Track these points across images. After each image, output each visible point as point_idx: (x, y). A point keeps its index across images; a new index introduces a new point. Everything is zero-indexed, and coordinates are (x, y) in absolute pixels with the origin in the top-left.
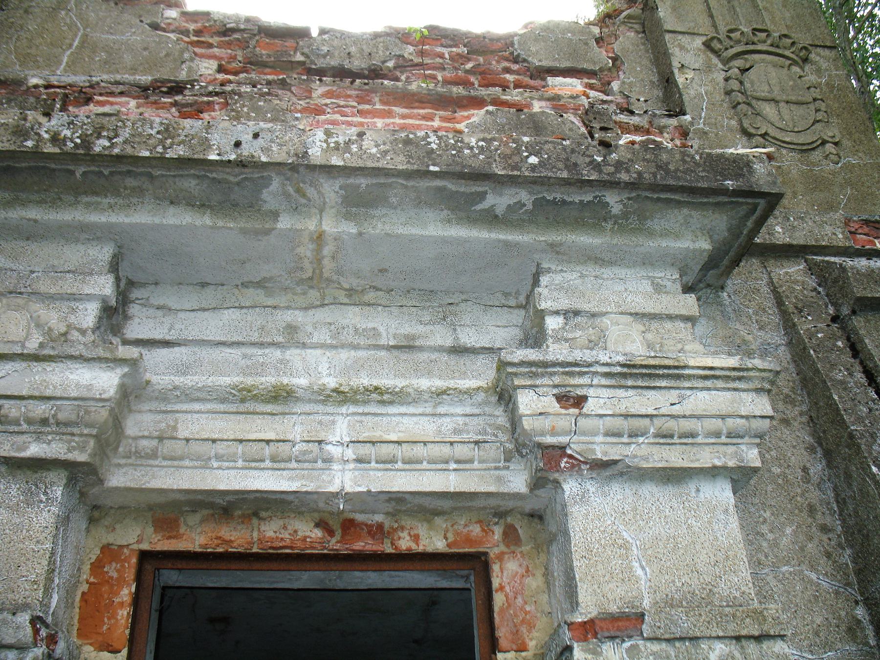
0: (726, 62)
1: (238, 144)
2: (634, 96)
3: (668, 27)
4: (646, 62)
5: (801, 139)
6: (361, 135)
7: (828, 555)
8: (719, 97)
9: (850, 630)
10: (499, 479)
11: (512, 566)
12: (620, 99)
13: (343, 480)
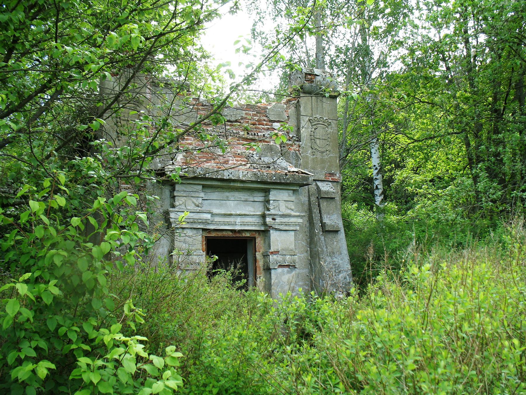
0: (312, 126)
4: (295, 118)
8: (308, 136)
11: (259, 239)
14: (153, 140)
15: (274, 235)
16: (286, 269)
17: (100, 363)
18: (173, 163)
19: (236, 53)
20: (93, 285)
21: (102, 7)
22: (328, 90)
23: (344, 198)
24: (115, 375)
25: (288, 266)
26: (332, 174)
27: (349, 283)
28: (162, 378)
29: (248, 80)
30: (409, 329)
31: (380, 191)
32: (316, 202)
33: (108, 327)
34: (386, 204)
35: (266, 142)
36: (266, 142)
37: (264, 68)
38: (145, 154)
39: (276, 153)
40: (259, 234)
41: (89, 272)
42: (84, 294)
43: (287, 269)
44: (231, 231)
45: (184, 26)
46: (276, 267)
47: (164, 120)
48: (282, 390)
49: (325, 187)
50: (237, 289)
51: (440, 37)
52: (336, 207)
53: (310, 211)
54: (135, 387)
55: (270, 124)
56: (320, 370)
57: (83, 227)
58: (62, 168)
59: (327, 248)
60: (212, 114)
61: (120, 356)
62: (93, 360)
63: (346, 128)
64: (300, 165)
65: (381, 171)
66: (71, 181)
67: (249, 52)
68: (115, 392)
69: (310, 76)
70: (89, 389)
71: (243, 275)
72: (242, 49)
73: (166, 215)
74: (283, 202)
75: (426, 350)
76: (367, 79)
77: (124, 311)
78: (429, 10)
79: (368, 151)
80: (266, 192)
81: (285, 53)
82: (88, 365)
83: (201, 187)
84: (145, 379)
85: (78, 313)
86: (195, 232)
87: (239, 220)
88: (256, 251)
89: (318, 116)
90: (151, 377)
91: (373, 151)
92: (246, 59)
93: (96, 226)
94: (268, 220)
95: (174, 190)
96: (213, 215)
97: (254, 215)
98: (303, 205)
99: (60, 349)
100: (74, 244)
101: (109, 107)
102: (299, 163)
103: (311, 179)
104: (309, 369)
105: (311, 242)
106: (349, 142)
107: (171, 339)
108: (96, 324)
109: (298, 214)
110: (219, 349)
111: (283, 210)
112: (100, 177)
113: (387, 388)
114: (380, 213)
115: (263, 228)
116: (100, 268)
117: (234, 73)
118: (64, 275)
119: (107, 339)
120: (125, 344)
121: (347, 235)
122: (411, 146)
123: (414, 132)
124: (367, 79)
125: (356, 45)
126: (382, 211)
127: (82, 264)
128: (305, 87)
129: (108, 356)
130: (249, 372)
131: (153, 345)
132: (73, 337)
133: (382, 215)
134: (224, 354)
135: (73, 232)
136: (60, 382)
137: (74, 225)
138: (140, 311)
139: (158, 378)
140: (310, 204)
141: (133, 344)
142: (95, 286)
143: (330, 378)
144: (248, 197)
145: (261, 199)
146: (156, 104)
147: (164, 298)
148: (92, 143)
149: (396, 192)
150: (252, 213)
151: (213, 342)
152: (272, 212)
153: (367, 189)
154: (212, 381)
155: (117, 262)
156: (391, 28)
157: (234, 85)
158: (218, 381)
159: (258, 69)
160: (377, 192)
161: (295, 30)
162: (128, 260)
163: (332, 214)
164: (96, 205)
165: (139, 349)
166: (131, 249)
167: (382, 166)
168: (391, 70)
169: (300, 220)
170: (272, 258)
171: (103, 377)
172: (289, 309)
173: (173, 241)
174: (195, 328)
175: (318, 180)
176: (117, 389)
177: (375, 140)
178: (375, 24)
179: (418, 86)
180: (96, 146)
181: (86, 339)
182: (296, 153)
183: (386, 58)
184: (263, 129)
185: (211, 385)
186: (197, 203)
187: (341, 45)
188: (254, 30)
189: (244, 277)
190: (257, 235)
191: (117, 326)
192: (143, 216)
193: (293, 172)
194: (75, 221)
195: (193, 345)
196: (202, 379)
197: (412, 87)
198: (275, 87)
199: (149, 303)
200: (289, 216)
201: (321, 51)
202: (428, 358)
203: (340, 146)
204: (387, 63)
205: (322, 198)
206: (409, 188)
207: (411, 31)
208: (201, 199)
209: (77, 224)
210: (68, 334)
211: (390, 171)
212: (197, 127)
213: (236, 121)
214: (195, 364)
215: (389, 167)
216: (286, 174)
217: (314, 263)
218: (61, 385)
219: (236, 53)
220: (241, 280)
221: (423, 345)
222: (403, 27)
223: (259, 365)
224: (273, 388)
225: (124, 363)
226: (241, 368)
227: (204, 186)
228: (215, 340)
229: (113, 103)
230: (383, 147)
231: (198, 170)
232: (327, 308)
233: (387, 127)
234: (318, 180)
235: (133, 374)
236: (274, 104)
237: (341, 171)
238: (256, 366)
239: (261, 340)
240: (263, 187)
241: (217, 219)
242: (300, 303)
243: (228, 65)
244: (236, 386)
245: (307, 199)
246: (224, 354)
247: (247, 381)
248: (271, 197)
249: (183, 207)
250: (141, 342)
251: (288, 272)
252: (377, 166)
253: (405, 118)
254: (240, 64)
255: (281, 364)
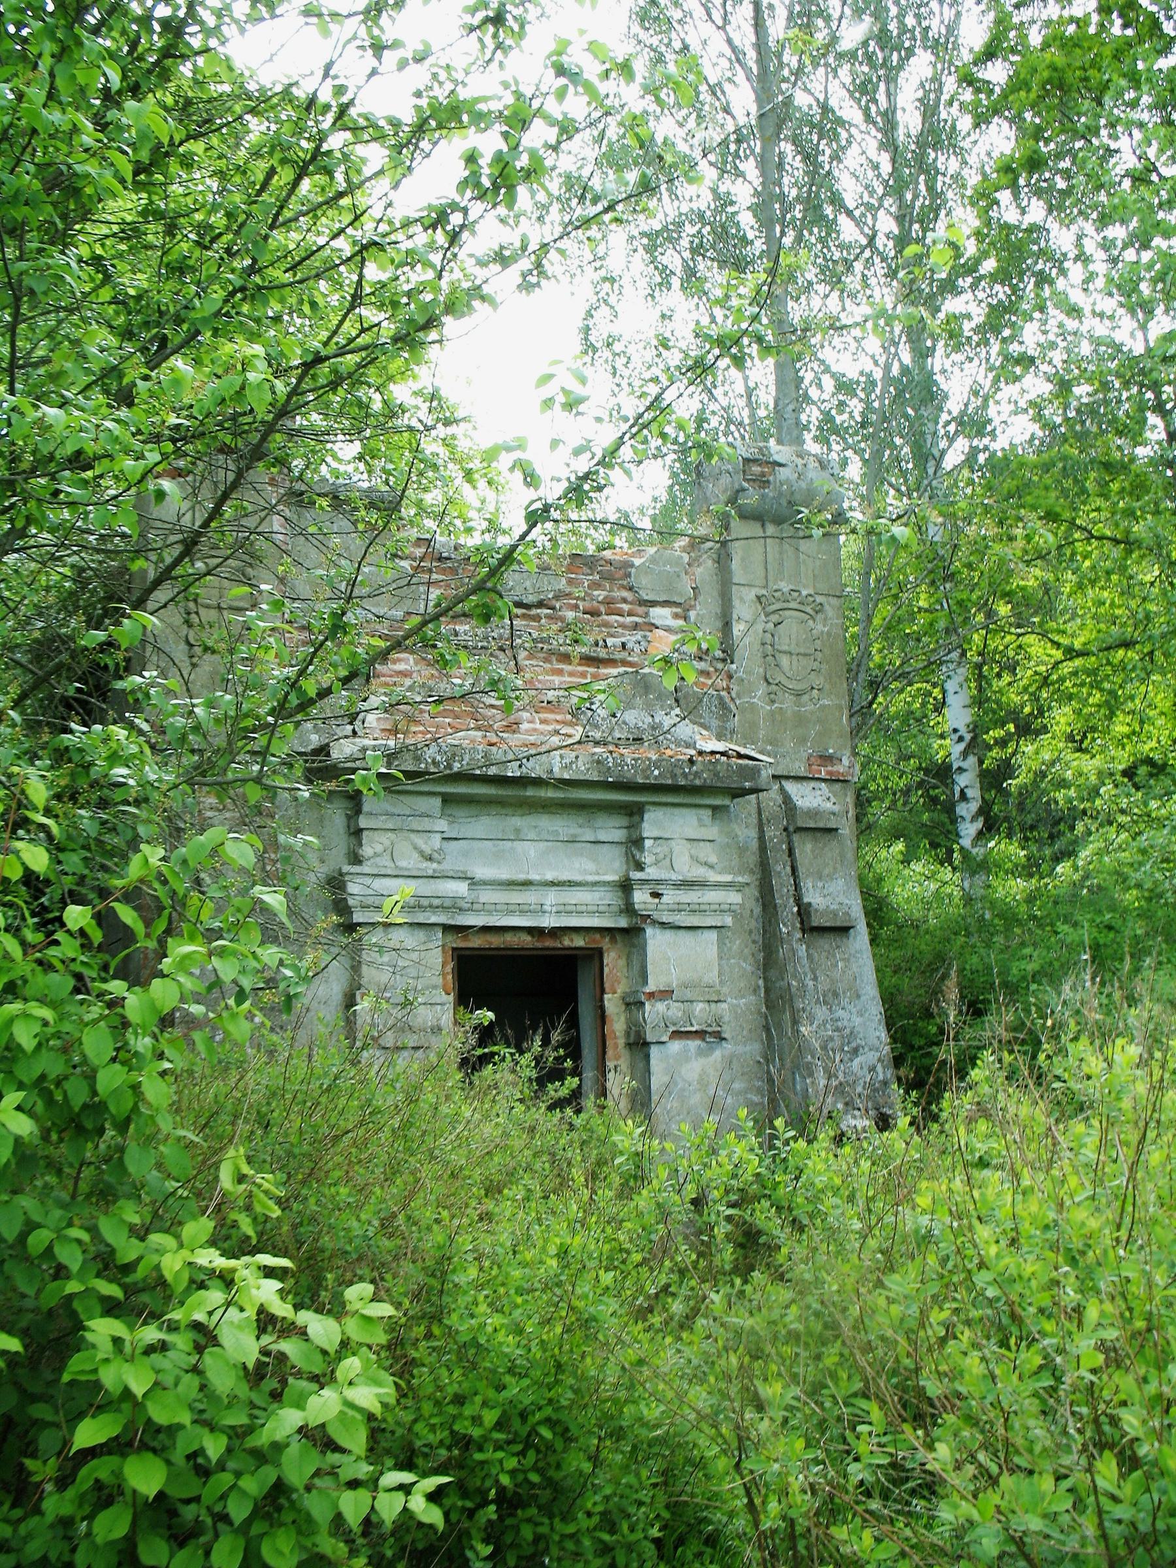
5: (799, 687)
8: (757, 646)
11: (613, 954)
14: (302, 673)
15: (655, 939)
16: (693, 1044)
17: (151, 1334)
18: (354, 733)
19: (543, 412)
20: (130, 1105)
21: (142, 280)
22: (819, 518)
23: (865, 829)
24: (195, 1370)
25: (700, 1034)
26: (827, 759)
27: (885, 1083)
28: (333, 1379)
29: (579, 491)
30: (1077, 1244)
31: (974, 806)
32: (781, 842)
33: (173, 1227)
34: (992, 844)
35: (631, 664)
36: (631, 664)
37: (626, 452)
38: (272, 712)
39: (660, 697)
40: (613, 940)
41: (117, 1066)
42: (101, 1131)
43: (698, 1042)
44: (530, 930)
45: (388, 329)
46: (665, 1038)
47: (333, 614)
48: (687, 1411)
49: (807, 797)
50: (551, 1108)
51: (1146, 341)
52: (842, 856)
53: (764, 870)
54: (253, 1406)
55: (641, 610)
56: (804, 1354)
57: (97, 936)
58: (32, 757)
59: (815, 979)
60: (473, 592)
61: (210, 1313)
62: (131, 1327)
63: (869, 618)
64: (733, 732)
65: (975, 745)
66: (58, 797)
67: (581, 408)
68: (195, 1422)
69: (758, 468)
70: (118, 1410)
71: (568, 1064)
72: (561, 399)
73: (336, 883)
74: (682, 843)
75: (1130, 1309)
76: (931, 471)
77: (217, 1179)
78: (1114, 261)
79: (934, 685)
80: (631, 815)
81: (686, 404)
82: (117, 1341)
83: (437, 802)
84: (284, 1382)
85: (83, 1187)
86: (421, 935)
87: (551, 898)
88: (603, 991)
89: (785, 586)
90: (299, 1374)
91: (950, 686)
92: (574, 429)
93: (139, 927)
94: (640, 897)
95: (358, 811)
96: (473, 883)
97: (595, 884)
98: (742, 850)
99: (31, 1292)
100: (71, 983)
101: (165, 576)
102: (729, 725)
103: (766, 774)
104: (768, 1349)
105: (769, 959)
106: (877, 659)
107: (360, 1259)
108: (136, 1220)
109: (728, 878)
110: (502, 1290)
111: (685, 868)
112: (145, 784)
113: (1016, 1423)
114: (973, 873)
115: (623, 923)
116: (149, 1055)
117: (538, 471)
118: (43, 1077)
119: (172, 1264)
120: (227, 1280)
121: (873, 941)
122: (1067, 668)
123: (1070, 627)
124: (931, 471)
125: (895, 370)
126: (975, 867)
127: (96, 1044)
128: (749, 501)
129: (176, 1315)
130: (588, 1360)
131: (305, 1280)
132: (71, 1257)
133: (980, 879)
134: (516, 1306)
135: (68, 948)
136: (30, 1389)
137: (73, 925)
138: (267, 1181)
139: (321, 1380)
140: (763, 848)
141: (252, 1280)
142: (135, 1109)
143: (834, 1376)
144: (579, 831)
145: (619, 835)
146: (311, 565)
147: (336, 1139)
148: (119, 685)
149: (1021, 807)
150: (590, 878)
151: (481, 1269)
152: (651, 872)
153: (934, 800)
154: (481, 1385)
155: (197, 1036)
156: (999, 318)
157: (538, 505)
158: (501, 1388)
159: (608, 459)
160: (962, 810)
161: (720, 342)
162: (231, 1028)
163: (831, 877)
164: (135, 869)
165: (267, 1292)
166: (241, 996)
167: (976, 729)
168: (1000, 445)
169: (735, 898)
170: (654, 1011)
171: (160, 1377)
172: (709, 1173)
173: (356, 968)
174: (429, 1229)
175: (787, 778)
176: (202, 1411)
177: (955, 655)
178: (952, 305)
179: (1084, 491)
180: (133, 691)
181: (106, 1262)
182: (721, 698)
183: (985, 405)
184: (623, 626)
185: (478, 1399)
186: (428, 851)
187: (852, 374)
188: (587, 330)
189: (569, 1072)
190: (605, 943)
191: (200, 1227)
192: (274, 899)
193: (713, 753)
194: (76, 916)
195: (421, 1278)
196: (453, 1381)
197: (1064, 493)
198: (655, 500)
199: (290, 1154)
200: (702, 884)
201: (790, 388)
202: (1135, 1334)
203: (853, 670)
204: (989, 421)
205: (799, 830)
206: (1060, 795)
207: (1061, 325)
208: (438, 836)
209: (82, 923)
210: (57, 1249)
211: (1002, 743)
212: (429, 631)
213: (540, 604)
214: (429, 1336)
215: (998, 733)
216: (691, 761)
217: (779, 1026)
218: (34, 1398)
219: (543, 412)
220: (562, 1079)
221: (1122, 1293)
222: (1037, 315)
223: (619, 1338)
224: (662, 1408)
225: (226, 1336)
226: (566, 1347)
227: (447, 800)
228: (487, 1264)
229: (177, 562)
230: (981, 675)
231: (431, 753)
232: (820, 1162)
233: (990, 614)
234: (787, 778)
235: (250, 1366)
236: (652, 550)
237: (854, 748)
238: (613, 1341)
239: (624, 1262)
240: (622, 800)
241: (487, 896)
242: (742, 1153)
243: (519, 447)
244: (550, 1401)
245: (753, 833)
246: (516, 1306)
247: (584, 1385)
248: (649, 828)
249: (385, 861)
250: (269, 1272)
251: (701, 1053)
252: (963, 731)
253: (1045, 584)
254: (555, 444)
255: (684, 1335)
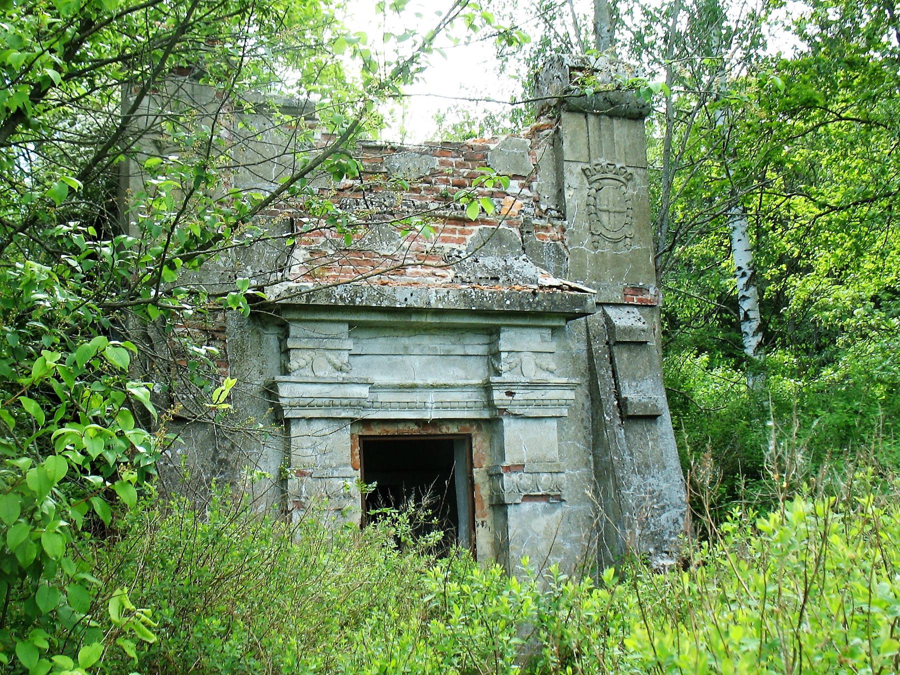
1: (406, 300)
2: (542, 194)
3: (566, 158)
4: (551, 168)
6: (448, 292)
7: (585, 437)
8: (583, 207)
9: (586, 464)
10: (481, 414)
11: (479, 439)
12: (536, 196)
13: (430, 415)
59: (632, 454)
